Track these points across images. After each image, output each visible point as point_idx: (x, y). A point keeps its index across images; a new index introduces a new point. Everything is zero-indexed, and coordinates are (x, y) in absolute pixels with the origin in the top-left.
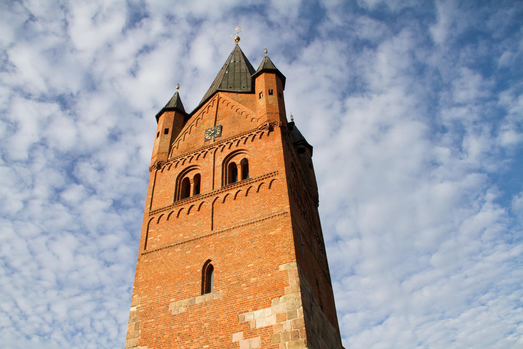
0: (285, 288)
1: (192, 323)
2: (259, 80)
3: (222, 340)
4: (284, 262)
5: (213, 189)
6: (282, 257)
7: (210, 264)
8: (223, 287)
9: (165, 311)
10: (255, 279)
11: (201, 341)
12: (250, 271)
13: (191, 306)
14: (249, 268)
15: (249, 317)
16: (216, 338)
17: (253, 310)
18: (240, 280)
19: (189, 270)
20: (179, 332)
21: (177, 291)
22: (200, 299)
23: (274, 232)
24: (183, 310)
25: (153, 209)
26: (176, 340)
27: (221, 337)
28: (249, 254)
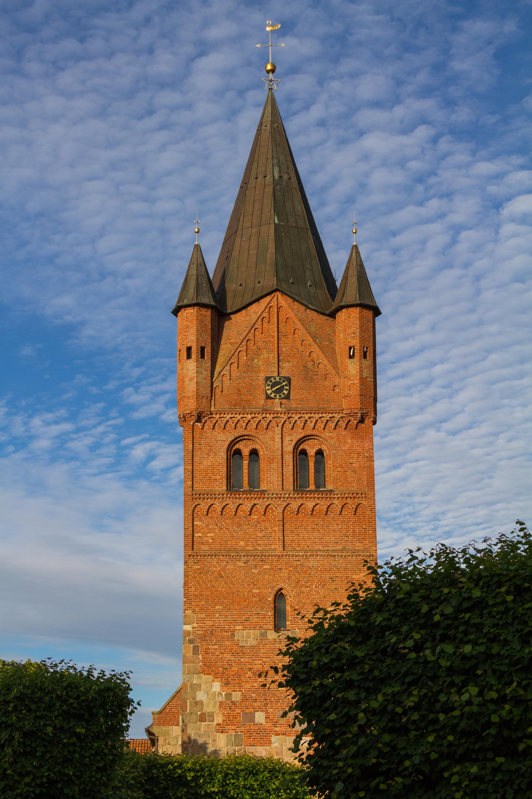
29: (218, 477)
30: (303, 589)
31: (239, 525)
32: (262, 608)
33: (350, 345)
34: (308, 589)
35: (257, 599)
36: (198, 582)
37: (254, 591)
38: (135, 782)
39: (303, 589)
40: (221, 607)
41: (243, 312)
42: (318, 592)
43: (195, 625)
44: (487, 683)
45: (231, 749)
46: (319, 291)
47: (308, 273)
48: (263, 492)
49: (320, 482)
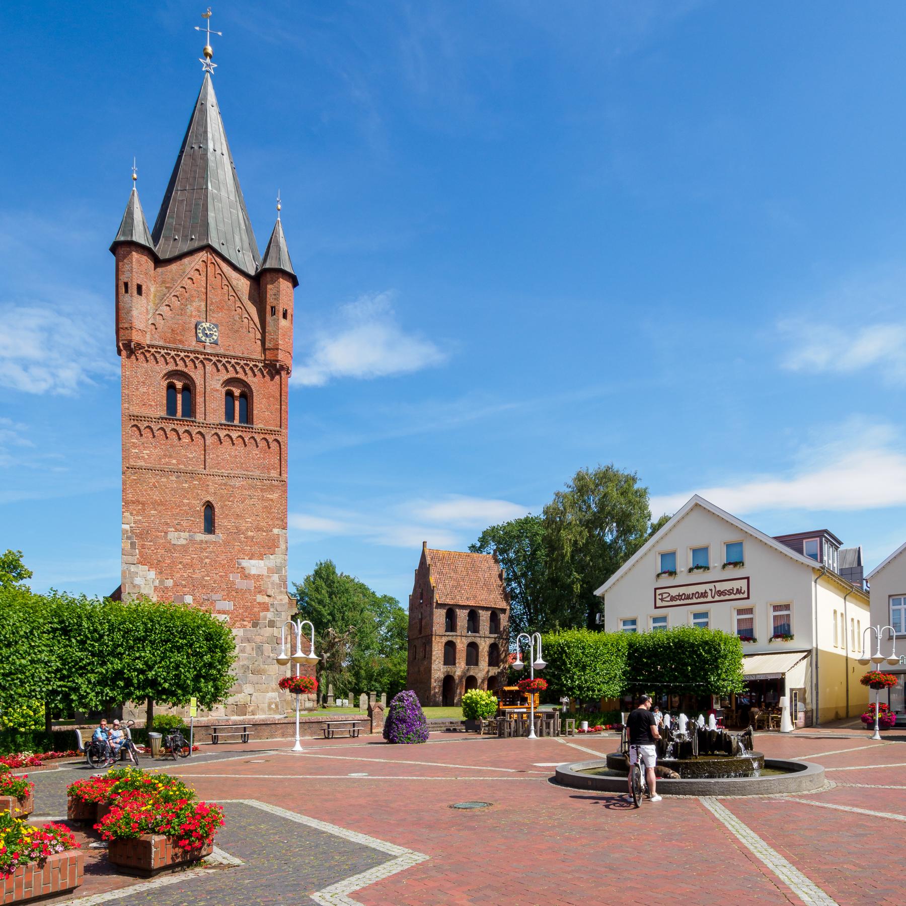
0: (276, 549)
1: (192, 556)
2: (245, 285)
3: (221, 576)
4: (278, 526)
5: (420, 633)
6: (277, 522)
7: (182, 417)
8: (223, 532)
9: (166, 537)
10: (252, 533)
11: (202, 573)
12: (247, 525)
13: (192, 540)
14: (247, 522)
15: (245, 563)
16: (216, 574)
17: (249, 559)
18: (239, 531)
19: (188, 504)
20: (181, 561)
21: (176, 522)
22: (201, 537)
23: (272, 496)
24: (183, 542)
25: (267, 266)
26: (178, 567)
27: (220, 574)
28: (247, 509)
43: (132, 525)
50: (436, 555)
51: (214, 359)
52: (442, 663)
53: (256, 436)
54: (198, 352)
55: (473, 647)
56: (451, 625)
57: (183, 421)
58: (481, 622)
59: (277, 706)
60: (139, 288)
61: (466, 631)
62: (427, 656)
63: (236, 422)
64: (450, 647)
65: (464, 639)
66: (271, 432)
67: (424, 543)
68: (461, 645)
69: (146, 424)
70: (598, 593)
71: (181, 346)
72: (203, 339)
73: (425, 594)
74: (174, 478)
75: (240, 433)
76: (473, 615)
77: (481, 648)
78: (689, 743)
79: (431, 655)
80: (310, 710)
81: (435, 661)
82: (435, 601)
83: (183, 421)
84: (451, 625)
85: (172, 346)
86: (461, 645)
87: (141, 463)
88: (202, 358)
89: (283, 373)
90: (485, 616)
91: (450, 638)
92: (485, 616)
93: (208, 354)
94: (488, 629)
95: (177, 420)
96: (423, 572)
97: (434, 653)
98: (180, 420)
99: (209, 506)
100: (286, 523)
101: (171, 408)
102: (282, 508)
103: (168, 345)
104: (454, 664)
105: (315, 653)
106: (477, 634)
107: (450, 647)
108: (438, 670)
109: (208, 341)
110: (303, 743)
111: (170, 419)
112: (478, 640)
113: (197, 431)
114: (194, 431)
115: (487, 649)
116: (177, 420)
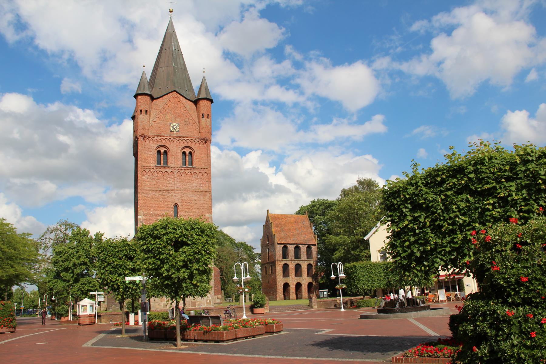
29: (152, 160)
30: (184, 204)
31: (160, 179)
32: (169, 210)
33: (202, 113)
34: (186, 203)
35: (167, 206)
36: (144, 200)
37: (166, 204)
38: (103, 288)
39: (184, 204)
40: (153, 210)
41: (161, 98)
42: (189, 205)
43: (143, 216)
44: (77, 275)
45: (17, 38)
46: (190, 93)
47: (186, 86)
48: (169, 167)
49: (191, 164)
50: (277, 218)
51: (178, 139)
52: (282, 276)
53: (197, 171)
54: (171, 136)
55: (298, 267)
56: (285, 255)
57: (164, 167)
58: (302, 253)
59: (210, 301)
60: (146, 111)
61: (294, 258)
62: (274, 272)
63: (187, 166)
64: (286, 267)
65: (293, 262)
66: (203, 169)
67: (268, 211)
68: (292, 266)
69: (149, 170)
70: (366, 238)
71: (163, 134)
72: (173, 130)
73: (270, 238)
74: (160, 193)
75: (189, 171)
76: (297, 248)
77: (303, 267)
78: (404, 302)
79: (276, 271)
80: (219, 304)
81: (278, 275)
82: (276, 242)
83: (164, 167)
84: (285, 255)
85: (160, 135)
86: (292, 266)
87: (147, 188)
88: (172, 138)
89: (208, 142)
90: (303, 249)
91: (285, 262)
92: (303, 249)
93: (175, 137)
94: (306, 256)
95: (162, 167)
96: (267, 226)
97: (277, 271)
98: (163, 167)
99: (176, 206)
100: (212, 211)
101: (159, 162)
102: (210, 204)
103: (158, 134)
104: (289, 276)
105: (249, 275)
106: (300, 259)
107: (286, 267)
108: (280, 281)
109: (175, 131)
110: (247, 316)
111: (159, 167)
112: (300, 263)
113: (170, 171)
114: (169, 171)
115: (306, 267)
116: (162, 167)
